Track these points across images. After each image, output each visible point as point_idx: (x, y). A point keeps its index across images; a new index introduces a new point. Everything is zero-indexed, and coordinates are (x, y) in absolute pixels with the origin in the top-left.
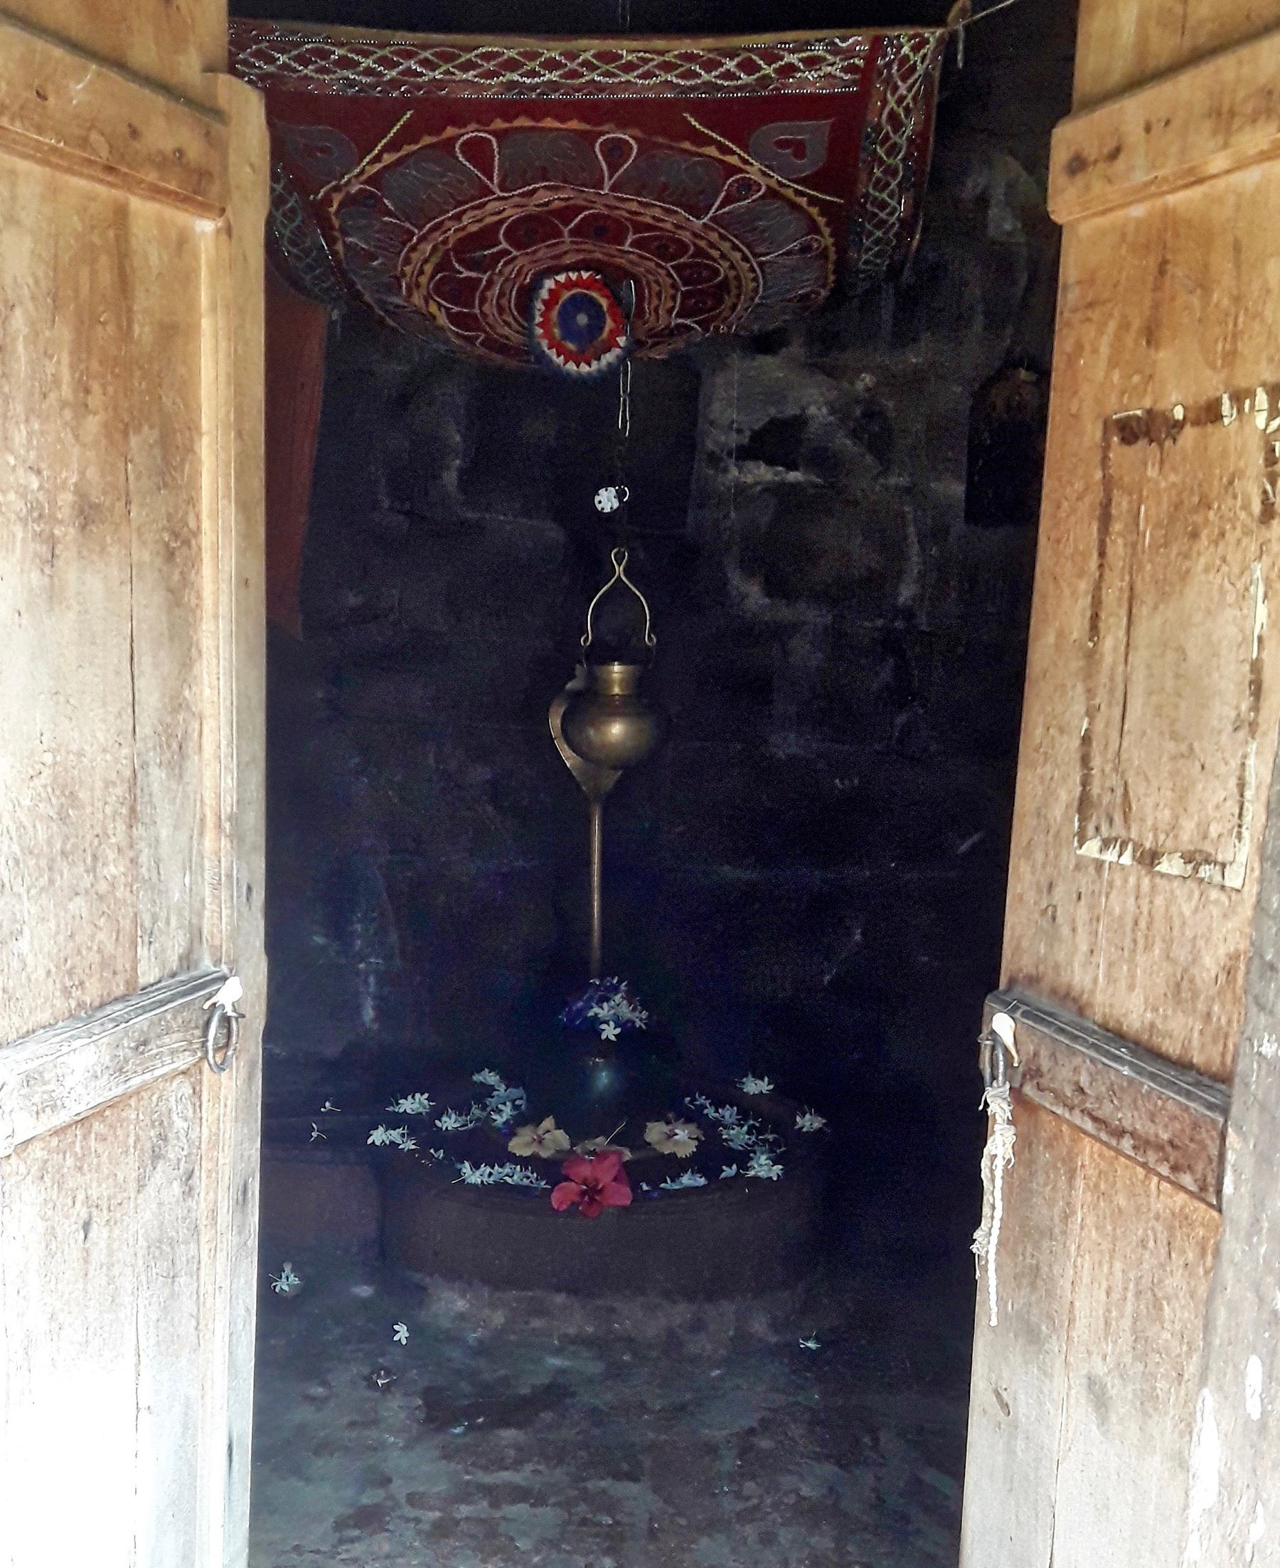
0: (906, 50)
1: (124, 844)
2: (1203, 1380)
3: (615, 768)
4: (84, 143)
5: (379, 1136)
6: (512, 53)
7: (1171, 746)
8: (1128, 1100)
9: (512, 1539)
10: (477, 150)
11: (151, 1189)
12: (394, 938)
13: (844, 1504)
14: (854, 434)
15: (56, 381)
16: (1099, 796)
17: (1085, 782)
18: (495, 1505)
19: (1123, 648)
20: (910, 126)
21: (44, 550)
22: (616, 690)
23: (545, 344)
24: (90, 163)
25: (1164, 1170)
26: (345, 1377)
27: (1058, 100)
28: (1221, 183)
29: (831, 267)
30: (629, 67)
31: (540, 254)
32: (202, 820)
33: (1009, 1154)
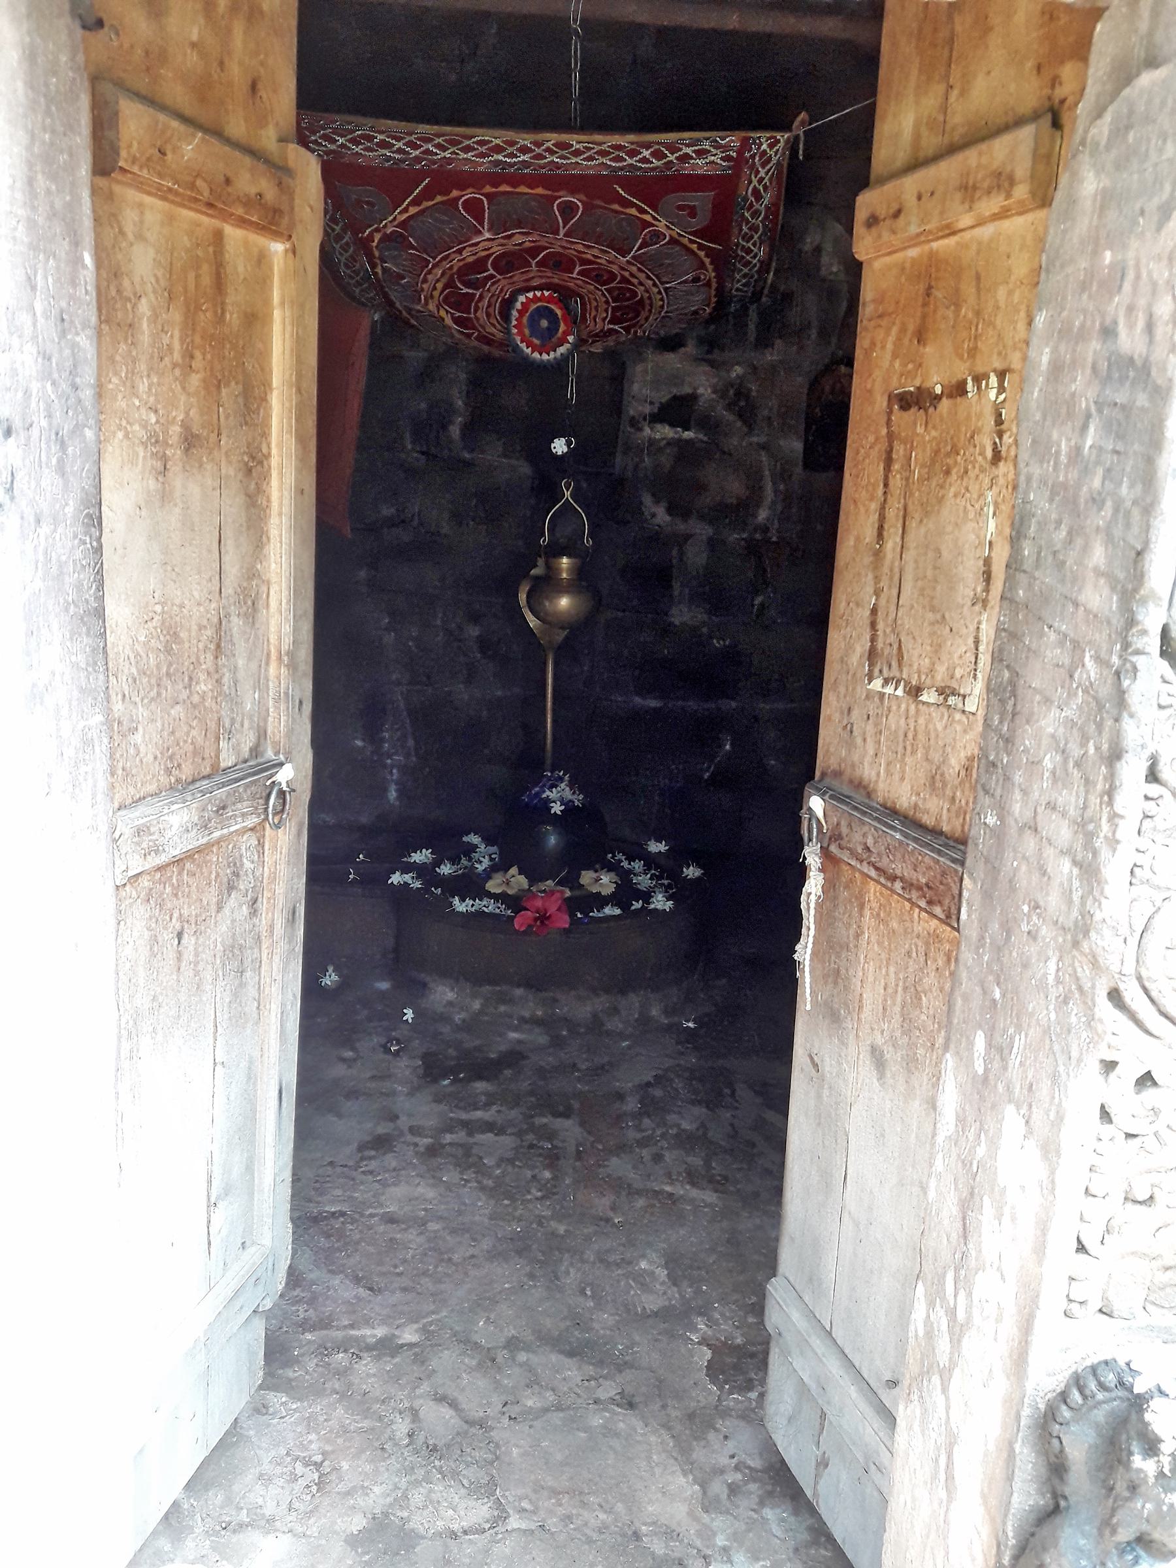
0: (764, 147)
1: (212, 670)
2: (946, 1048)
3: (563, 628)
4: (192, 186)
5: (396, 878)
6: (498, 141)
7: (930, 616)
8: (899, 855)
9: (481, 1158)
10: (474, 207)
11: (227, 911)
12: (411, 743)
13: (710, 1134)
14: (729, 407)
15: (170, 348)
16: (882, 649)
17: (873, 639)
18: (470, 1134)
19: (899, 549)
20: (767, 198)
21: (159, 465)
22: (564, 575)
23: (518, 339)
24: (196, 200)
25: (923, 904)
26: (370, 1043)
27: (862, 180)
28: (967, 235)
29: (713, 293)
30: (577, 153)
31: (515, 279)
32: (268, 655)
33: (820, 892)
